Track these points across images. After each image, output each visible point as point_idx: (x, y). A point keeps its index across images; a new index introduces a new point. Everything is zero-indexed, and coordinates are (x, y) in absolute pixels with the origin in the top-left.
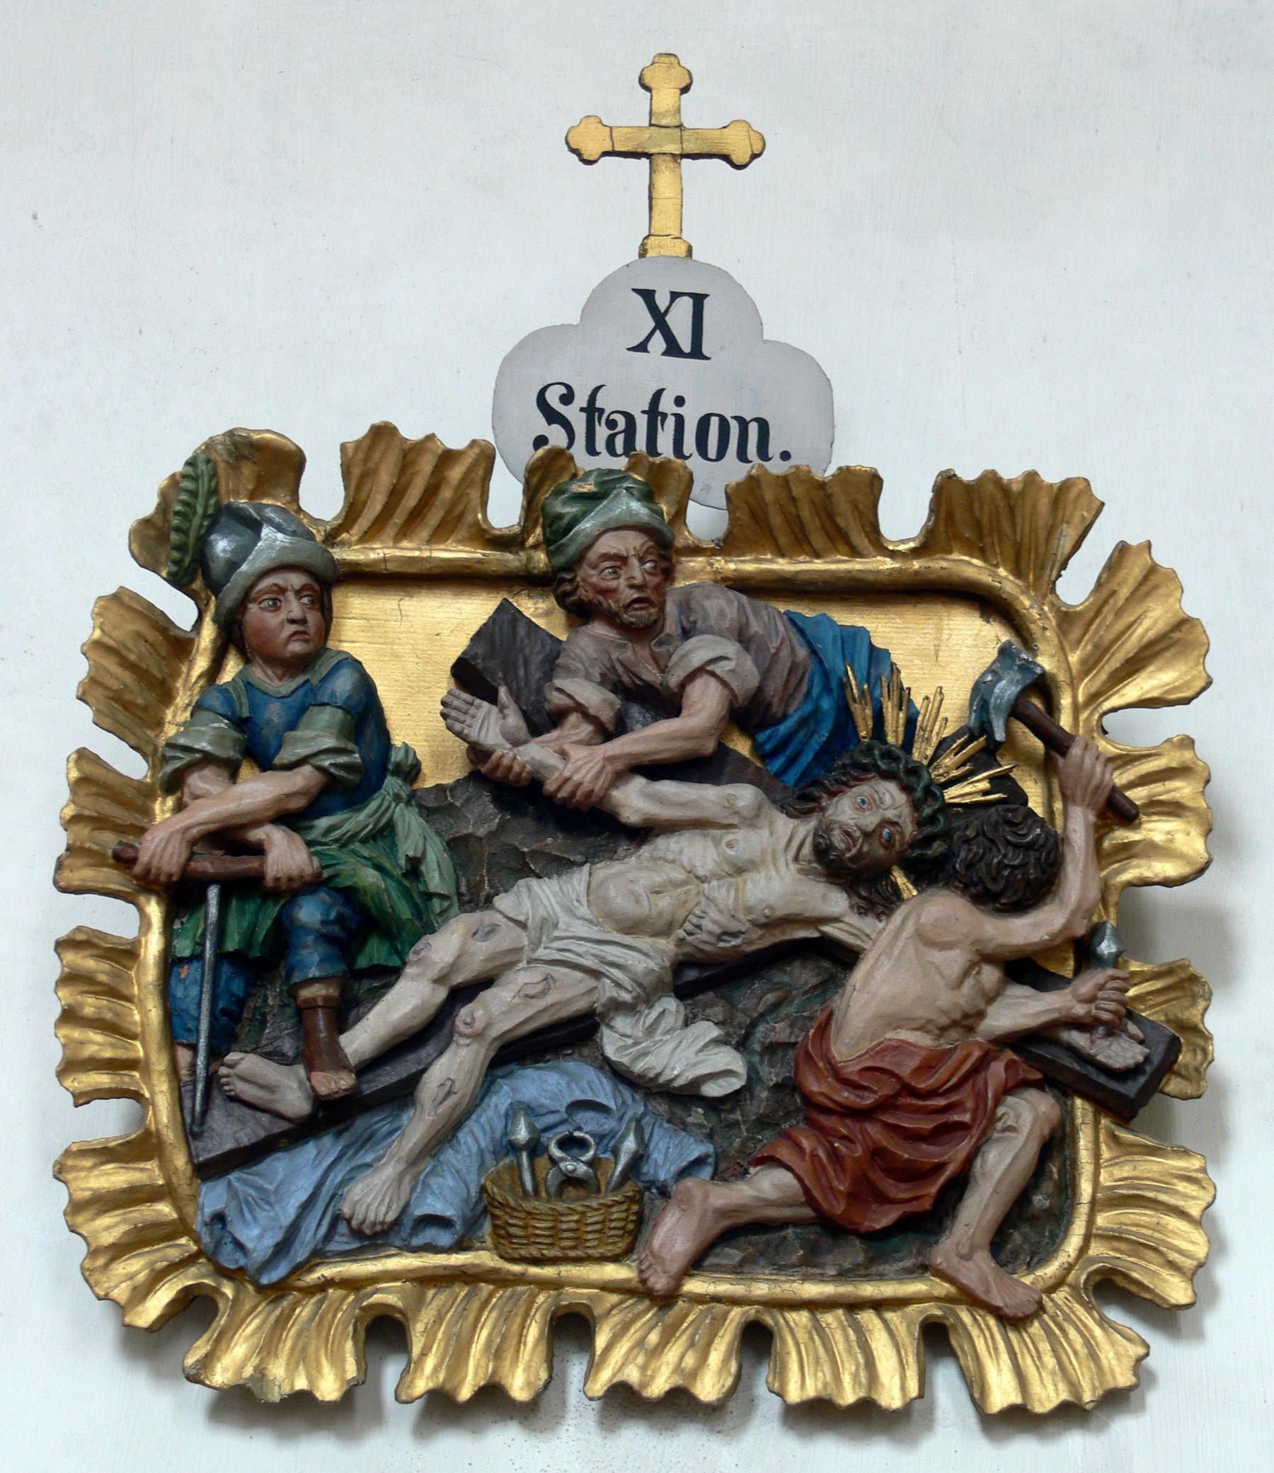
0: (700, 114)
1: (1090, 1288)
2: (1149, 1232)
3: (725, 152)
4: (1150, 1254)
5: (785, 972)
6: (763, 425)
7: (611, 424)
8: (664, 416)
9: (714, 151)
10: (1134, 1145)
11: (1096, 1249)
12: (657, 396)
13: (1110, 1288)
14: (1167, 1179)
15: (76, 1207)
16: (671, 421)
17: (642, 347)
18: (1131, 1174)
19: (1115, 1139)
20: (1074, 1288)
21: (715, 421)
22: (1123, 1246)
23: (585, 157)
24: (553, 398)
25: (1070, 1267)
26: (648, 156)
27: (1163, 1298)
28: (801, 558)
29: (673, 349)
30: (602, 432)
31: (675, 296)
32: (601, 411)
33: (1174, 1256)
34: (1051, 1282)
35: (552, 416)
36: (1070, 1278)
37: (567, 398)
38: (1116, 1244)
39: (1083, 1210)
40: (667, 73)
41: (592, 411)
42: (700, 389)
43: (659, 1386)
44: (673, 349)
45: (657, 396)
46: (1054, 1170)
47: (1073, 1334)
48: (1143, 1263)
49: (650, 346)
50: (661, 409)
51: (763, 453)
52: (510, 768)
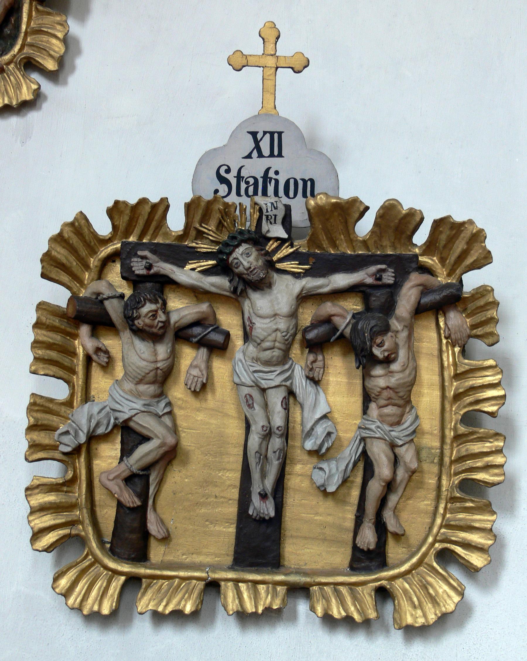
0: (254, 47)
1: (23, 64)
2: (45, 44)
4: (44, 52)
6: (312, 181)
7: (247, 183)
8: (271, 179)
10: (43, 12)
11: (26, 50)
13: (29, 65)
14: (53, 24)
15: (33, 511)
16: (273, 182)
17: (249, 156)
18: (41, 22)
19: (37, 10)
20: (16, 63)
21: (292, 182)
22: (35, 49)
24: (222, 172)
25: (15, 56)
27: (46, 68)
30: (243, 186)
31: (265, 133)
33: (52, 53)
34: (7, 61)
35: (223, 180)
36: (15, 60)
37: (228, 171)
38: (33, 48)
39: (22, 35)
40: (271, 35)
41: (239, 177)
42: (286, 168)
46: (13, 20)
47: (12, 78)
48: (42, 55)
50: (269, 176)
51: (313, 195)
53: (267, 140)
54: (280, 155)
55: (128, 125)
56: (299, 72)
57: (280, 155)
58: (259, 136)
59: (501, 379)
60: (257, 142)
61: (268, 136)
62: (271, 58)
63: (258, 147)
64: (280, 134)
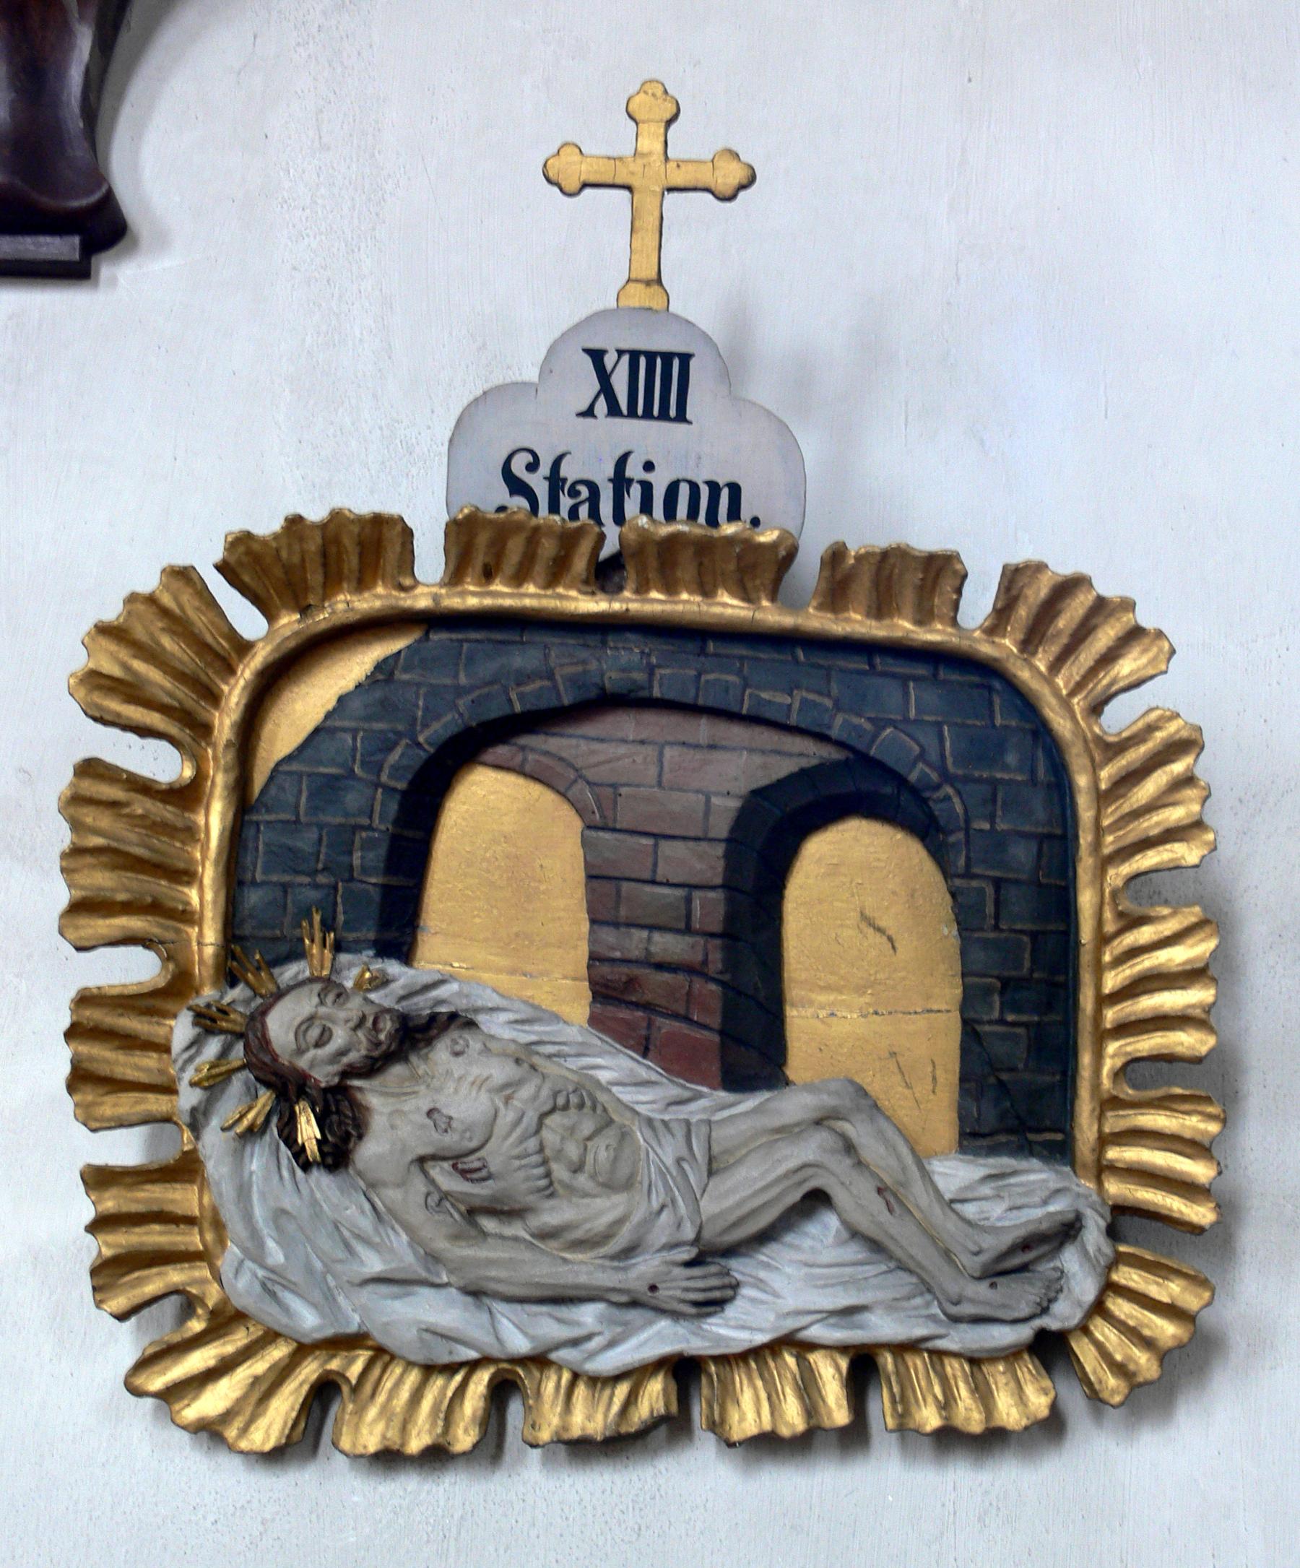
3: (707, 185)
5: (806, 1234)
6: (735, 489)
7: (573, 493)
8: (630, 481)
9: (700, 185)
12: (622, 462)
16: (636, 490)
21: (684, 490)
23: (551, 175)
24: (518, 467)
26: (629, 188)
28: (1102, 675)
29: (614, 410)
31: (620, 353)
32: (565, 480)
35: (516, 486)
37: (532, 467)
41: (555, 481)
42: (666, 451)
43: (415, 1445)
44: (614, 410)
45: (622, 462)
49: (596, 412)
52: (738, 1367)
53: (655, 381)
54: (681, 417)
55: (304, 315)
56: (731, 198)
57: (681, 417)
58: (609, 360)
59: (844, 1223)
60: (604, 377)
61: (626, 358)
62: (656, 172)
63: (606, 389)
64: (685, 359)
